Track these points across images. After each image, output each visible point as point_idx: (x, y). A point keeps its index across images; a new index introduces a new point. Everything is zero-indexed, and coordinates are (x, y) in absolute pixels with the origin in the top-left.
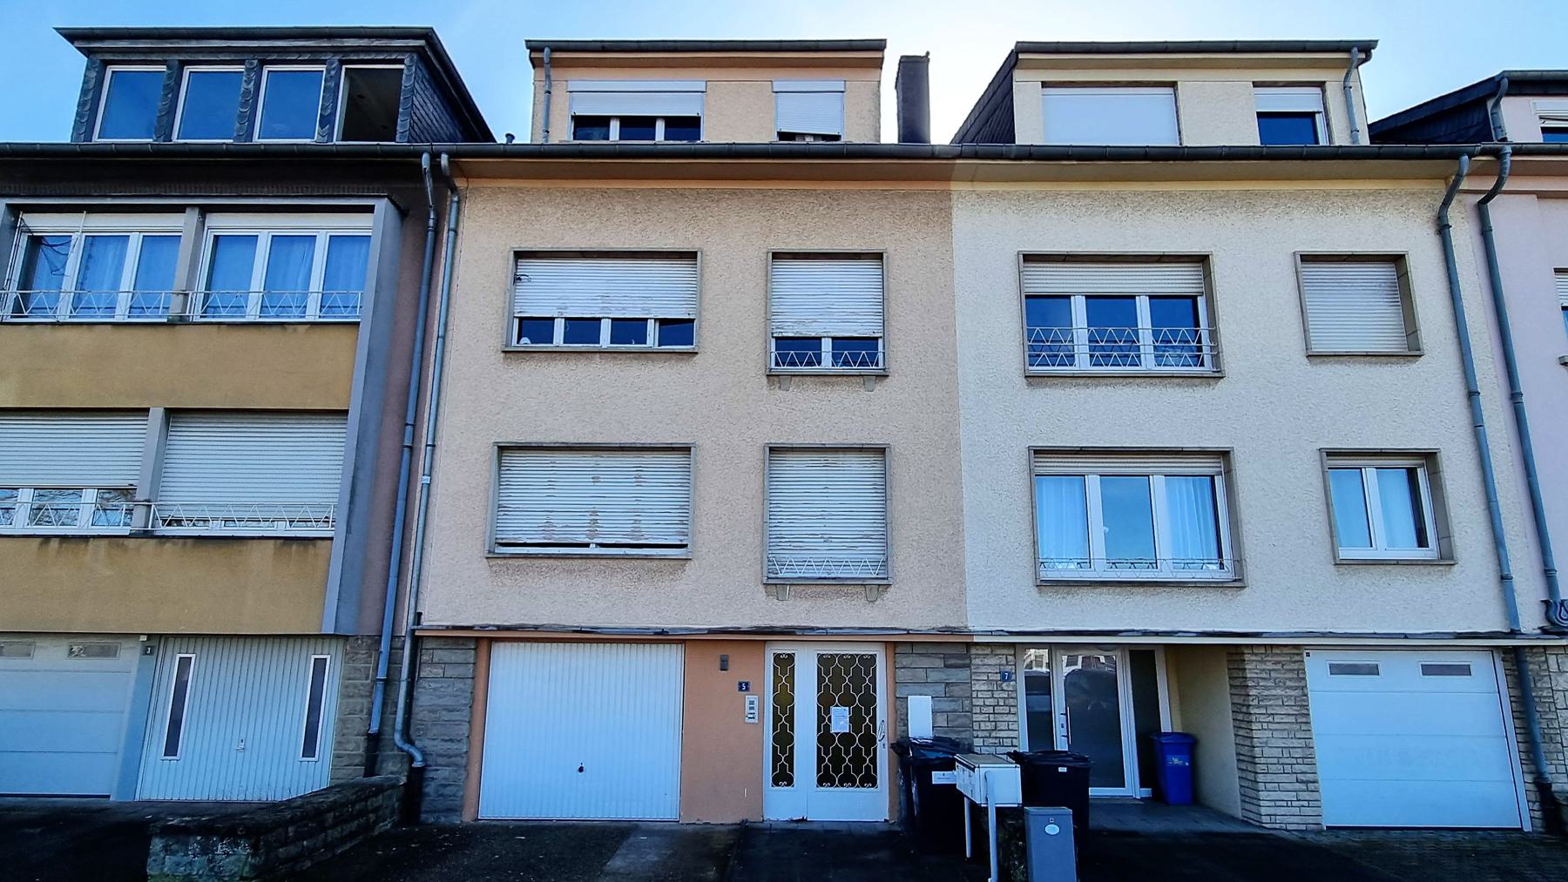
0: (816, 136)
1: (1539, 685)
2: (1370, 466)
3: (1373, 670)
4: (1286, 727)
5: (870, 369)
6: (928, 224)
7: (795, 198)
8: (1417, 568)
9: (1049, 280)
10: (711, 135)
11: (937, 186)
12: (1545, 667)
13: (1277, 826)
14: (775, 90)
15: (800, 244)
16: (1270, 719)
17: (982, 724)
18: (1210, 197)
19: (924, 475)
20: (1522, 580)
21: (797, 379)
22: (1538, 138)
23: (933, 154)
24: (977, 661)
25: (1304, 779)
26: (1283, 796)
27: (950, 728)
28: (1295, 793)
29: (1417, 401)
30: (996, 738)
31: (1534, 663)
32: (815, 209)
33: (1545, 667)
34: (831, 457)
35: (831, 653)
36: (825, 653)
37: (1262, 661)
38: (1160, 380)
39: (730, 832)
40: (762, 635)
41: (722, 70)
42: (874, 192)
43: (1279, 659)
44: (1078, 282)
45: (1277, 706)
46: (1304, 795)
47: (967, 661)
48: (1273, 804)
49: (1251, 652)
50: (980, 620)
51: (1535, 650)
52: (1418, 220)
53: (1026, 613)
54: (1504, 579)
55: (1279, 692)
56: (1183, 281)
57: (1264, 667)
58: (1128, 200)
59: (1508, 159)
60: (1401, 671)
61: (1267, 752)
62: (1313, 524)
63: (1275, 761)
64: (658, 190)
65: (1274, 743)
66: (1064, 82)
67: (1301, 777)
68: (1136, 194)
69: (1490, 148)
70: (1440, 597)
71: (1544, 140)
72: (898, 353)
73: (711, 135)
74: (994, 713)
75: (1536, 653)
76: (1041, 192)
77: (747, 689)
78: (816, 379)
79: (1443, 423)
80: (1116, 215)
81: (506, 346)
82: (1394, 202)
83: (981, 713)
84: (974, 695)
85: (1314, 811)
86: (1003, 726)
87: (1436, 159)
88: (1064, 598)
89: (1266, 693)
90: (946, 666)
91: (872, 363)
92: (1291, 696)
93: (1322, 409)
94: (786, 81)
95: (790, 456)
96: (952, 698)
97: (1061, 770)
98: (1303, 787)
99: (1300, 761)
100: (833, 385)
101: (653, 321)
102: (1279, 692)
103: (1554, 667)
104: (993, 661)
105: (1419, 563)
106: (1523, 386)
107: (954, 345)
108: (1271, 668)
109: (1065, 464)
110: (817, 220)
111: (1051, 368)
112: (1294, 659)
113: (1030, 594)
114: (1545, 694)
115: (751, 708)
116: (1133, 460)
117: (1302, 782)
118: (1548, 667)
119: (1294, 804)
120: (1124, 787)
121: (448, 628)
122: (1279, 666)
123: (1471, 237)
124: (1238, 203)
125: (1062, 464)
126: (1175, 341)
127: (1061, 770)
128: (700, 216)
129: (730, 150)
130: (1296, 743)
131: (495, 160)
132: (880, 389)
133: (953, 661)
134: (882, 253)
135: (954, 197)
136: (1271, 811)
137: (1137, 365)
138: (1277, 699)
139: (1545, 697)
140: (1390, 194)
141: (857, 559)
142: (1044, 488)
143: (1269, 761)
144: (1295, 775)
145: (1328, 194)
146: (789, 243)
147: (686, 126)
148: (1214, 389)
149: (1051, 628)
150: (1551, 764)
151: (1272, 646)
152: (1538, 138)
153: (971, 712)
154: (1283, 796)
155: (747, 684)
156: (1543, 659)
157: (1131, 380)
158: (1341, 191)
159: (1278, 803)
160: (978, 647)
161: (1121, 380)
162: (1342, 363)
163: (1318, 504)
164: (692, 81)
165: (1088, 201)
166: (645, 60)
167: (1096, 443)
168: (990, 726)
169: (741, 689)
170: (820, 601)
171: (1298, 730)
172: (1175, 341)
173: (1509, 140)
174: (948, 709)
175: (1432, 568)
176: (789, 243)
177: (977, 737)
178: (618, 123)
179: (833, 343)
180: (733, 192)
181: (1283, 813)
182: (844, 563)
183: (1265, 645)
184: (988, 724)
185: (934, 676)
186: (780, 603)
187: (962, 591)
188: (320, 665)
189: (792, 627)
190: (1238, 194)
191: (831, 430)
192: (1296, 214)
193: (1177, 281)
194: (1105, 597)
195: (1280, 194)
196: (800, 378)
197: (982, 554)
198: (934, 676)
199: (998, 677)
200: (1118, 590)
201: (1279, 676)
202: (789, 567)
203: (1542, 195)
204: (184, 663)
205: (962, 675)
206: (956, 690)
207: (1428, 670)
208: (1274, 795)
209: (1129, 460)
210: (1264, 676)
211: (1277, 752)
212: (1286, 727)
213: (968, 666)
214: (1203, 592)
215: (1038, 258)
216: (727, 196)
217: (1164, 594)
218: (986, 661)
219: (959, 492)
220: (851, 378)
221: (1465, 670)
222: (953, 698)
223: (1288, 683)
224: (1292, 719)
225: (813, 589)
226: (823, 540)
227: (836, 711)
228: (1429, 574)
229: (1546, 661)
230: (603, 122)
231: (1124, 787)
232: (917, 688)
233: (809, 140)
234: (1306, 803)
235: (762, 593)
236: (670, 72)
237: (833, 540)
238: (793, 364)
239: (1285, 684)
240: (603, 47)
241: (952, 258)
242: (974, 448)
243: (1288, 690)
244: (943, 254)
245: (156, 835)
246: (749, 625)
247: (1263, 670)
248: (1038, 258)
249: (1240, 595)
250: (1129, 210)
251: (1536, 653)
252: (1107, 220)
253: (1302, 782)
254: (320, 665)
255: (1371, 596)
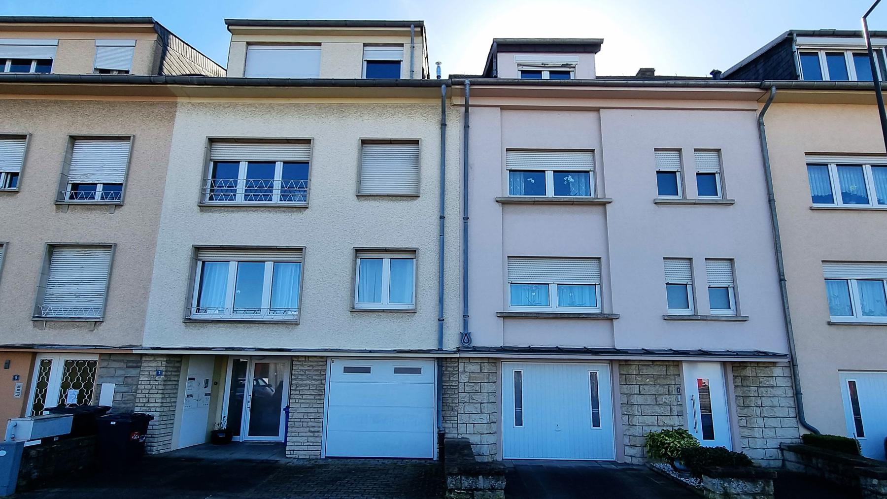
0: (120, 71)
1: (451, 379)
2: (386, 257)
3: (367, 370)
4: (308, 401)
5: (116, 201)
6: (161, 120)
7: (90, 106)
8: (396, 314)
9: (224, 153)
10: (56, 70)
11: (170, 100)
12: (456, 369)
13: (294, 456)
14: (96, 45)
15: (88, 131)
16: (300, 397)
17: (141, 399)
18: (320, 107)
19: (133, 261)
20: (453, 321)
21: (72, 207)
22: (518, 76)
23: (151, 81)
24: (144, 364)
25: (313, 430)
26: (299, 439)
27: (124, 402)
28: (306, 438)
29: (413, 222)
30: (147, 407)
31: (451, 367)
32: (100, 111)
33: (456, 369)
34: (88, 250)
35: (72, 359)
36: (69, 359)
37: (302, 365)
38: (274, 209)
39: (414, 466)
40: (30, 351)
41: (62, 33)
42: (133, 103)
43: (312, 364)
44: (244, 154)
45: (306, 390)
46: (310, 439)
47: (139, 364)
48: (293, 444)
49: (297, 360)
50: (149, 341)
51: (452, 360)
52: (433, 121)
53: (176, 338)
54: (441, 320)
55: (308, 382)
56: (304, 154)
57: (303, 368)
58: (275, 109)
59: (467, 87)
60: (383, 371)
61: (296, 415)
62: (343, 290)
63: (299, 420)
64: (15, 100)
65: (300, 410)
66: (310, 43)
67: (312, 429)
68: (280, 105)
69: (458, 81)
70: (406, 330)
71: (521, 77)
72: (131, 195)
73: (56, 70)
74: (149, 393)
75: (453, 362)
76: (227, 103)
77: (18, 379)
78: (83, 207)
79: (425, 234)
80: (267, 117)
81: (359, 193)
82: (421, 111)
83: (141, 393)
84: (140, 383)
85: (315, 448)
86: (152, 400)
87: (377, 86)
88: (199, 329)
89: (301, 383)
90: (128, 367)
91: (116, 198)
92: (315, 384)
93: (360, 225)
94: (104, 40)
95: (67, 250)
96: (129, 386)
97: (112, 423)
98: (312, 434)
99: (312, 420)
100: (92, 209)
101: (4, 173)
102: (308, 382)
103: (461, 369)
104: (154, 364)
105: (396, 311)
106: (471, 215)
107: (164, 188)
108: (306, 369)
109: (282, 256)
110: (100, 118)
111: (225, 201)
112: (319, 364)
113: (180, 327)
114: (453, 384)
115: (18, 390)
116: (283, 254)
117: (311, 432)
118: (458, 369)
119: (306, 444)
120: (249, 435)
121: (120, 348)
122: (311, 368)
123: (460, 131)
124: (335, 111)
125: (278, 256)
126: (296, 188)
127: (112, 423)
128: (35, 114)
129: (36, 78)
130: (312, 410)
131: (33, 84)
132: (118, 212)
133: (130, 364)
134: (418, 140)
135: (179, 105)
136: (292, 448)
137: (233, 200)
138: (306, 386)
139: (453, 386)
140: (420, 106)
141: (87, 307)
142: (218, 267)
143: (296, 420)
144: (308, 428)
145: (386, 106)
146: (82, 131)
147: (45, 64)
148: (303, 214)
149: (187, 346)
150: (450, 423)
151: (308, 356)
152: (518, 76)
153: (136, 392)
154: (299, 439)
155: (18, 376)
156: (456, 365)
157: (258, 209)
158: (393, 105)
159: (296, 444)
160: (147, 356)
161: (252, 208)
162: (375, 200)
163: (348, 278)
164: (51, 39)
165: (253, 109)
166: (283, 31)
167: (232, 243)
168: (145, 400)
169: (14, 379)
170: (62, 330)
171: (315, 403)
172: (225, 187)
173: (499, 77)
174: (124, 391)
175: (404, 314)
176: (82, 131)
177: (137, 406)
178: (10, 63)
179: (103, 186)
180: (56, 102)
181: (298, 449)
182: (79, 310)
183: (305, 356)
184: (144, 399)
185: (119, 372)
186: (40, 331)
187: (143, 326)
188: (594, 377)
189: (33, 345)
190: (336, 106)
191: (86, 235)
192: (366, 117)
193: (295, 154)
194: (222, 329)
195: (359, 105)
196: (74, 206)
197: (158, 305)
198: (119, 372)
199: (155, 373)
200: (229, 325)
201: (310, 373)
202: (70, 312)
203: (503, 108)
204: (518, 374)
205: (133, 372)
206: (129, 380)
207: (398, 371)
208: (295, 439)
209: (281, 254)
210: (302, 373)
211: (301, 416)
212: (308, 401)
213: (140, 367)
214: (276, 327)
215: (221, 140)
216: (52, 104)
217: (255, 327)
218: (150, 364)
219: (151, 270)
220: (103, 206)
221: (417, 371)
222: (126, 384)
223: (314, 377)
224: (312, 397)
225: (60, 323)
226: (75, 296)
227: (71, 392)
228: (402, 317)
229: (458, 366)
230: (28, 62)
231: (249, 435)
232: (109, 379)
233: (115, 73)
234: (311, 444)
235: (31, 325)
236: (116, 35)
237: (81, 296)
238: (82, 198)
239: (312, 377)
240: (308, 24)
241: (171, 140)
242: (164, 245)
243: (313, 381)
244: (167, 137)
245: (879, 482)
246: (21, 343)
247: (302, 370)
248: (221, 140)
249: (297, 328)
250: (274, 114)
251: (453, 362)
252: (262, 119)
253: (311, 432)
254: (594, 377)
255: (368, 329)
